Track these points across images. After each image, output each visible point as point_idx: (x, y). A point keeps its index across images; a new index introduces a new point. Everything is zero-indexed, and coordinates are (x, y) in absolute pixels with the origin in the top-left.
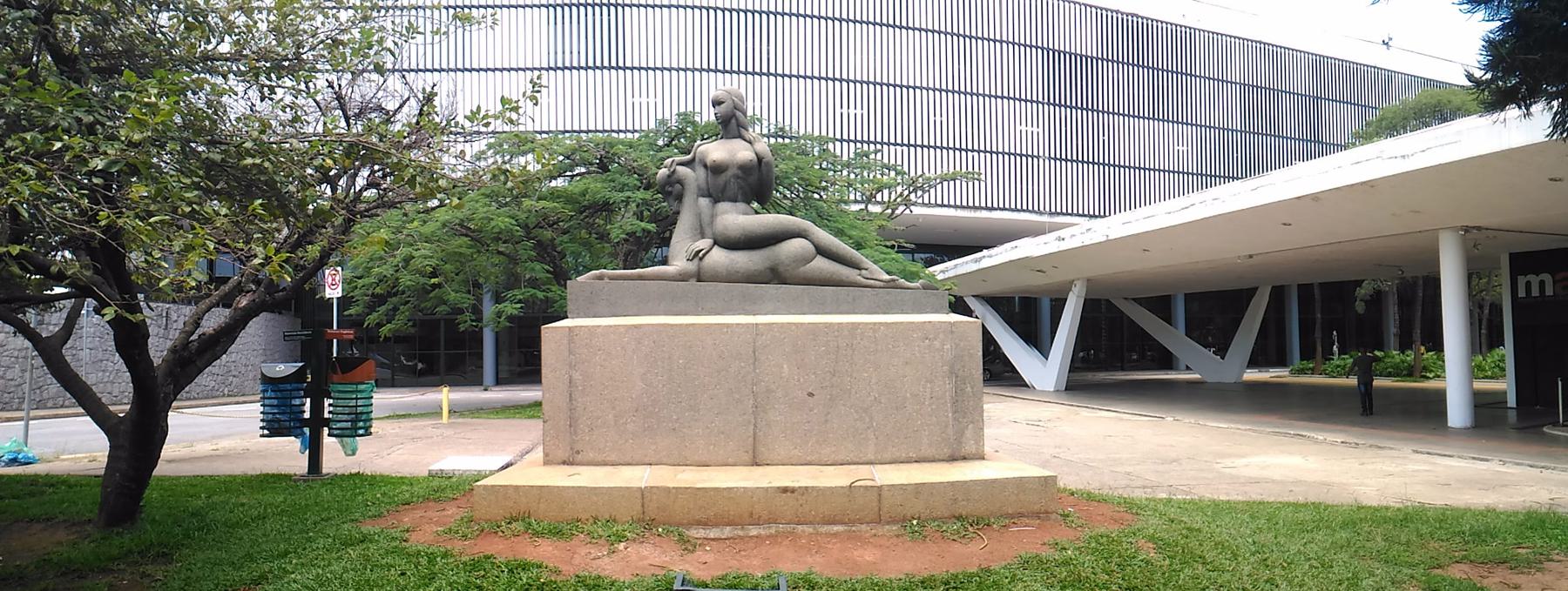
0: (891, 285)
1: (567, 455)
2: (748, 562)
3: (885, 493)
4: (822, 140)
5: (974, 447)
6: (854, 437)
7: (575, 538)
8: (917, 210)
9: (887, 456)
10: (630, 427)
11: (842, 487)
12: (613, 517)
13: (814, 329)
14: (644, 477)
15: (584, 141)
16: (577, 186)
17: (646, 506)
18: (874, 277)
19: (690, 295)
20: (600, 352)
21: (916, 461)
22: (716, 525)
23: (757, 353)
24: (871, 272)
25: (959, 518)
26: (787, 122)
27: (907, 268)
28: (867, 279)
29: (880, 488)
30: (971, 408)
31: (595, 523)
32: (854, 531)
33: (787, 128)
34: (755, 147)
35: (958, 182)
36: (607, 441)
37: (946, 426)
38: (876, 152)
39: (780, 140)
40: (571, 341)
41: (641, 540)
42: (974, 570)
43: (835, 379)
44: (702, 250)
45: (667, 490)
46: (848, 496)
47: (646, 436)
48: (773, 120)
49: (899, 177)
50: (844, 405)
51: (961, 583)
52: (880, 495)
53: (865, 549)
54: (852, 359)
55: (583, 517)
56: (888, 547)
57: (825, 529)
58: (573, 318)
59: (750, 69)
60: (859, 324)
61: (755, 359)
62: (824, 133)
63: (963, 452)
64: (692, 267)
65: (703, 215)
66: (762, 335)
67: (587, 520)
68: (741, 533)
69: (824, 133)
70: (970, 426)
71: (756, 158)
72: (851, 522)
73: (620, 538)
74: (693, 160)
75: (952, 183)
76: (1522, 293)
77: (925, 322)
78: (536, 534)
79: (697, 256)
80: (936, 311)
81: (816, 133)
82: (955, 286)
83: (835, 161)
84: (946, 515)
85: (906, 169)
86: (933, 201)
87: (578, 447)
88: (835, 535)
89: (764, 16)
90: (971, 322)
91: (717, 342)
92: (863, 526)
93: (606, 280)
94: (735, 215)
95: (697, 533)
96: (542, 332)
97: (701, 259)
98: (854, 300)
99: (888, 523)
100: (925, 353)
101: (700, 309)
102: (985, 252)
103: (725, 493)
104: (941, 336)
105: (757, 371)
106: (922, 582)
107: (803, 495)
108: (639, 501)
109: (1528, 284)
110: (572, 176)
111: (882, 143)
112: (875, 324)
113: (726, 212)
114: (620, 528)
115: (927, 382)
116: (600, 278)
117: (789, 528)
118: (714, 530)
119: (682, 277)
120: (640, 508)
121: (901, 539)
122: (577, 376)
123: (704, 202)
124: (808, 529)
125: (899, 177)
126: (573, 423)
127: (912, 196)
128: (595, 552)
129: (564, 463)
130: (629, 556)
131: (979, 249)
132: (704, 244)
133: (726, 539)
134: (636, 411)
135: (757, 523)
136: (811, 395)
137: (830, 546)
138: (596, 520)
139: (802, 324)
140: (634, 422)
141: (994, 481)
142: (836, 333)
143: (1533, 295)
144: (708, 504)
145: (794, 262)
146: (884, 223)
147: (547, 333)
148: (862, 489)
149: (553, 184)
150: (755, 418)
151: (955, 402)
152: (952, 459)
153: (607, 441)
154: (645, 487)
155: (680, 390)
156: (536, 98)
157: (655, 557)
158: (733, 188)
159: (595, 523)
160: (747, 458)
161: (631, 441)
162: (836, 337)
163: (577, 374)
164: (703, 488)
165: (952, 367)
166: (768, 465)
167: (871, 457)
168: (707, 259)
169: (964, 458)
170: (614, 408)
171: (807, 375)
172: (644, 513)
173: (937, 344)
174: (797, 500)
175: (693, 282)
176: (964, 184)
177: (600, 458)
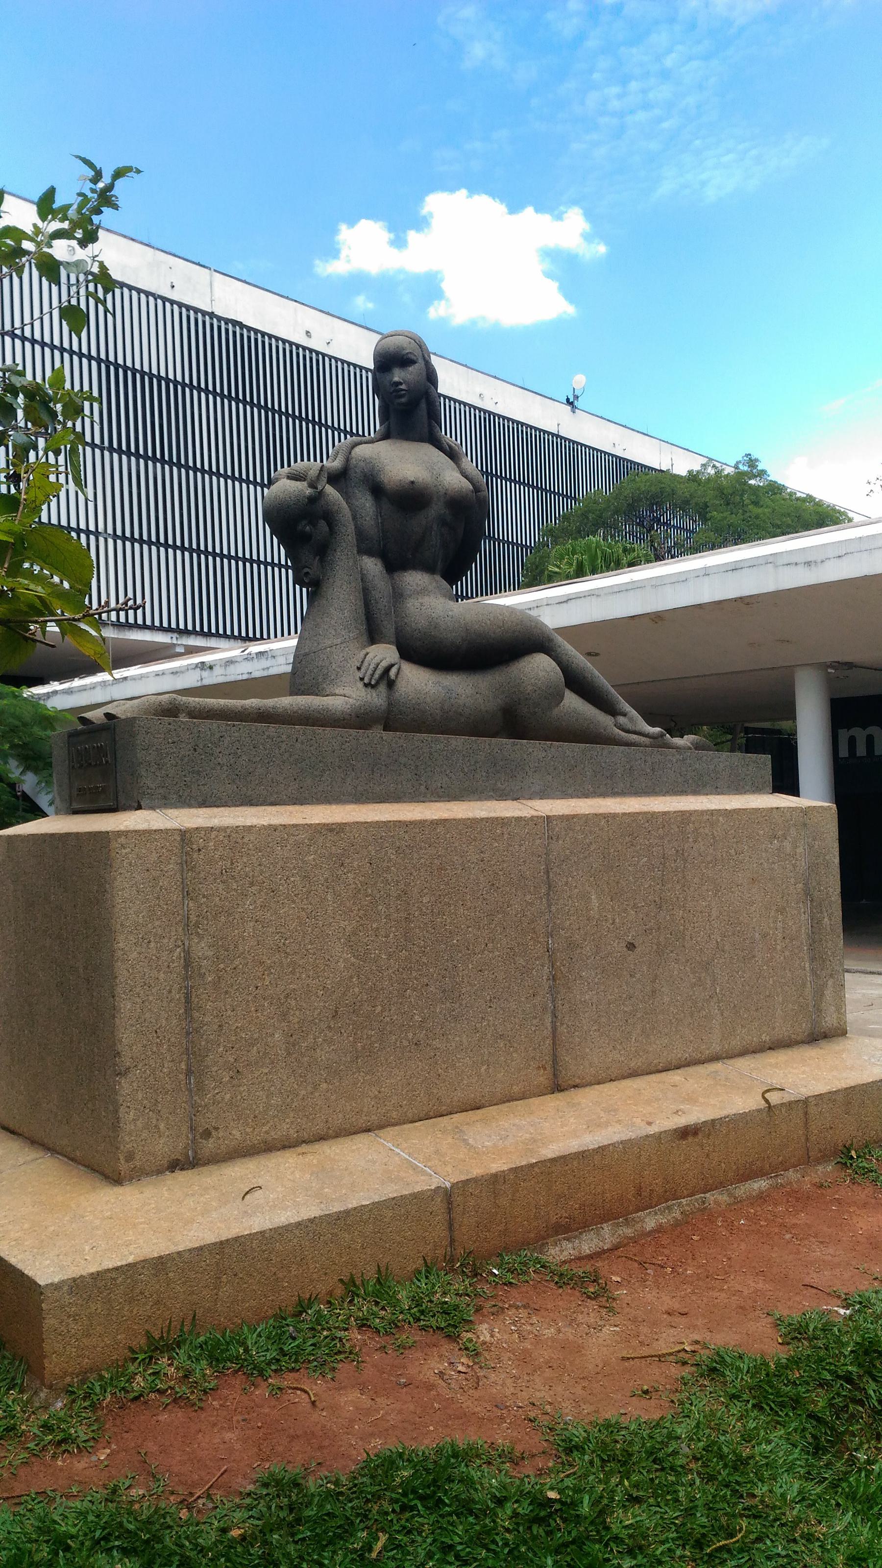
5: (835, 1016)
9: (736, 1043)
18: (638, 729)
19: (403, 760)
21: (770, 1048)
23: (551, 875)
24: (631, 720)
28: (628, 731)
29: (806, 1102)
36: (269, 1095)
37: (804, 985)
40: (186, 864)
46: (768, 1124)
50: (677, 961)
57: (744, 1189)
61: (550, 887)
64: (377, 699)
68: (628, 1231)
70: (830, 983)
76: (844, 753)
80: (757, 790)
87: (203, 1123)
91: (486, 855)
93: (183, 718)
105: (553, 908)
108: (441, 1217)
109: (852, 741)
113: (423, 592)
118: (584, 1237)
120: (445, 1233)
122: (202, 949)
123: (372, 566)
129: (175, 1166)
134: (335, 1016)
139: (614, 816)
140: (330, 1042)
142: (661, 831)
143: (858, 755)
151: (811, 948)
153: (269, 1095)
160: (542, 1079)
161: (324, 1086)
162: (662, 838)
166: (575, 1086)
167: (716, 1048)
170: (284, 1016)
172: (452, 1241)
173: (787, 845)
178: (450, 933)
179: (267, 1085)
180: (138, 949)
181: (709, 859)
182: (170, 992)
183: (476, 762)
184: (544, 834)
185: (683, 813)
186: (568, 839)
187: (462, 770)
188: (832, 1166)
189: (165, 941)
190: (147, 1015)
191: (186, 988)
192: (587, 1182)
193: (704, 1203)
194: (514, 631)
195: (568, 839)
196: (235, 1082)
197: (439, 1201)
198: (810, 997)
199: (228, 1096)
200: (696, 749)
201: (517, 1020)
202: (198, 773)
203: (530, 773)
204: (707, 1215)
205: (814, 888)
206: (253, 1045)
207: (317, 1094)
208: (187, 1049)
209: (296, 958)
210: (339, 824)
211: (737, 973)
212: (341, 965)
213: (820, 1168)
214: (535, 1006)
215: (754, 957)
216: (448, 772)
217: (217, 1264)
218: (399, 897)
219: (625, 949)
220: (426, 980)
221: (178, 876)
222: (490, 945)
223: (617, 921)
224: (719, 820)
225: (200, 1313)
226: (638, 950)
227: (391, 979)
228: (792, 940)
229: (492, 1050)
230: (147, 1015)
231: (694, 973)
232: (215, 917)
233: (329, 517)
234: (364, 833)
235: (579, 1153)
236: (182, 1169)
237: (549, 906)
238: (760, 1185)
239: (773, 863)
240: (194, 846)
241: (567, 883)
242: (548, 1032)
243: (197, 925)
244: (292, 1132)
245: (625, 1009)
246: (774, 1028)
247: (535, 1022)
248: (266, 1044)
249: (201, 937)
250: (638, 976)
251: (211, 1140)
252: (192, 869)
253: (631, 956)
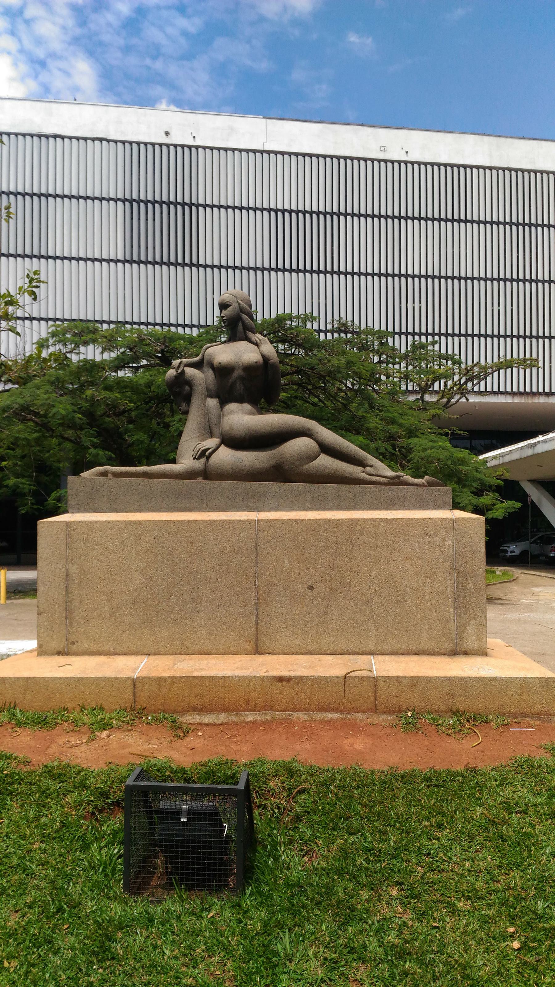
0: (396, 482)
1: (62, 646)
2: (238, 747)
3: (381, 684)
4: (381, 335)
6: (354, 628)
7: (58, 728)
8: (473, 399)
9: (387, 647)
10: (127, 619)
11: (337, 677)
12: (99, 706)
13: (314, 525)
14: (138, 667)
15: (145, 335)
16: (143, 377)
17: (137, 695)
18: (379, 473)
20: (97, 547)
21: (416, 654)
22: (211, 711)
24: (376, 469)
25: (456, 713)
26: (350, 318)
27: (455, 455)
29: (376, 679)
30: (473, 605)
31: (82, 711)
32: (349, 719)
33: (350, 324)
34: (261, 349)
35: (515, 370)
36: (102, 632)
37: (448, 621)
38: (434, 343)
39: (343, 335)
40: (68, 536)
41: (130, 728)
42: (460, 768)
43: (334, 573)
44: (209, 449)
45: (160, 680)
47: (145, 628)
48: (336, 317)
49: (456, 367)
51: (444, 781)
52: (376, 685)
53: (357, 738)
54: (351, 554)
55: (70, 706)
56: (380, 737)
57: (320, 716)
58: (73, 513)
59: (315, 268)
60: (358, 520)
61: (257, 554)
62: (383, 328)
63: (465, 647)
64: (199, 464)
65: (211, 416)
66: (263, 531)
67: (74, 709)
68: (235, 719)
69: (383, 328)
70: (473, 622)
71: (262, 358)
72: (348, 710)
73: (105, 725)
74: (202, 361)
75: (509, 371)
77: (425, 519)
78: (19, 724)
79: (203, 454)
81: (377, 328)
82: (508, 472)
83: (393, 354)
84: (443, 709)
85: (463, 359)
86: (489, 389)
87: (73, 638)
88: (330, 722)
89: (307, 216)
90: (474, 519)
92: (360, 714)
94: (240, 415)
95: (190, 719)
96: (39, 527)
97: (208, 458)
98: (355, 496)
99: (384, 713)
100: (425, 549)
101: (205, 505)
102: (540, 438)
103: (221, 682)
104: (443, 532)
105: (259, 565)
106: (402, 777)
107: (298, 684)
110: (137, 369)
111: (440, 335)
112: (375, 520)
113: (232, 412)
114: (107, 715)
115: (427, 577)
116: (104, 474)
117: (284, 715)
118: (208, 716)
119: (190, 475)
121: (394, 730)
122: (74, 570)
123: (213, 403)
124: (303, 716)
125: (456, 367)
126: (69, 615)
127: (469, 385)
128: (75, 740)
129: (59, 653)
130: (110, 744)
131: (534, 434)
132: (211, 443)
133: (220, 725)
135: (253, 708)
136: (311, 588)
137: (321, 733)
138: (82, 708)
139: (302, 520)
140: (132, 614)
141: (492, 680)
142: (335, 529)
144: (203, 692)
145: (298, 460)
146: (438, 412)
147: (42, 527)
148: (357, 680)
149: (121, 374)
150: (257, 609)
151: (456, 599)
152: (454, 653)
153: (102, 632)
154: (138, 678)
155: (181, 583)
156: (33, 293)
157: (139, 745)
158: (240, 388)
159: (82, 711)
160: (249, 646)
162: (334, 532)
163: (74, 568)
164: (199, 677)
165: (453, 564)
166: (269, 653)
167: (372, 647)
168: (213, 458)
169: (466, 653)
170: (110, 600)
171: (308, 569)
172: (135, 702)
173: (438, 540)
174: (293, 688)
175: (200, 479)
176: (522, 372)
177: (95, 648)
178: (197, 572)
179: (101, 628)
180: (47, 567)
181: (372, 545)
182: (59, 585)
183: (236, 493)
184: (255, 528)
185: (352, 520)
186: (270, 531)
187: (228, 497)
188: (393, 718)
189: (58, 565)
190: (50, 593)
191: (67, 584)
192: (214, 691)
193: (290, 716)
194: (279, 428)
195: (270, 531)
196: (86, 624)
197: (129, 683)
198: (453, 629)
199: (83, 630)
200: (429, 486)
201: (234, 617)
202: (93, 499)
203: (269, 498)
204: (288, 723)
205: (461, 566)
206: (95, 611)
207: (124, 635)
208: (66, 608)
209: (116, 577)
210: (140, 521)
211: (391, 609)
212: (138, 582)
213: (383, 717)
214: (245, 611)
215: (405, 601)
216: (219, 498)
217: (25, 685)
218: (169, 554)
219: (307, 589)
220: (182, 592)
221: (65, 540)
222: (219, 580)
223: (302, 574)
224: (380, 524)
225: (17, 702)
226: (316, 590)
227: (163, 590)
228: (438, 594)
229: (219, 629)
230: (50, 593)
231: (357, 605)
232: (80, 557)
233: (189, 383)
234: (152, 525)
235: (210, 677)
236: (62, 655)
237: (257, 563)
238: (335, 716)
239: (425, 549)
240: (72, 528)
241: (268, 553)
242: (253, 624)
243: (72, 560)
244: (111, 649)
245: (306, 619)
246: (420, 643)
247: (245, 619)
248: (101, 611)
249: (73, 565)
250: (315, 603)
251: (75, 646)
252: (70, 538)
253: (310, 593)
